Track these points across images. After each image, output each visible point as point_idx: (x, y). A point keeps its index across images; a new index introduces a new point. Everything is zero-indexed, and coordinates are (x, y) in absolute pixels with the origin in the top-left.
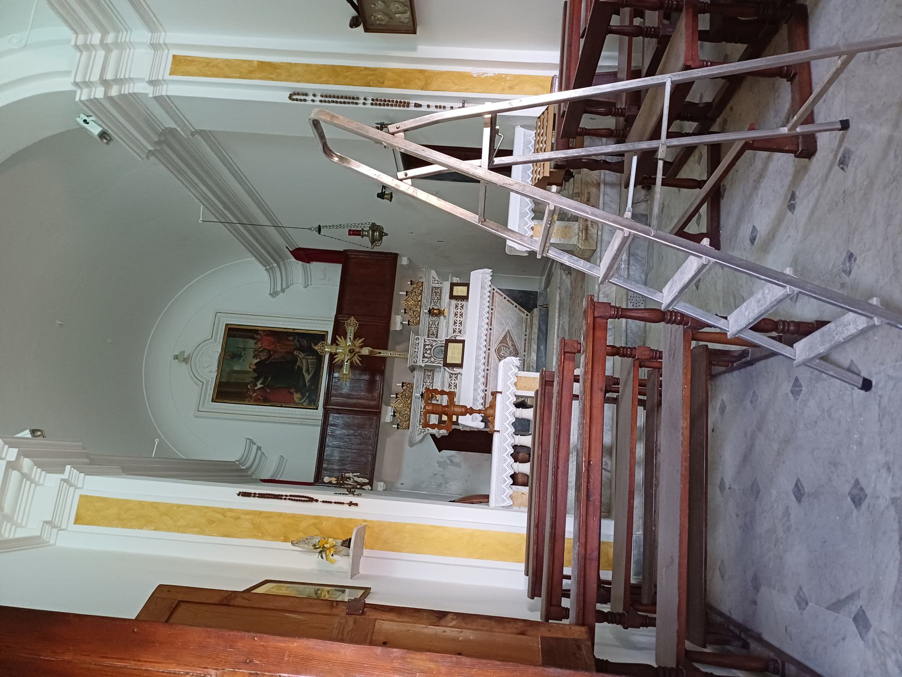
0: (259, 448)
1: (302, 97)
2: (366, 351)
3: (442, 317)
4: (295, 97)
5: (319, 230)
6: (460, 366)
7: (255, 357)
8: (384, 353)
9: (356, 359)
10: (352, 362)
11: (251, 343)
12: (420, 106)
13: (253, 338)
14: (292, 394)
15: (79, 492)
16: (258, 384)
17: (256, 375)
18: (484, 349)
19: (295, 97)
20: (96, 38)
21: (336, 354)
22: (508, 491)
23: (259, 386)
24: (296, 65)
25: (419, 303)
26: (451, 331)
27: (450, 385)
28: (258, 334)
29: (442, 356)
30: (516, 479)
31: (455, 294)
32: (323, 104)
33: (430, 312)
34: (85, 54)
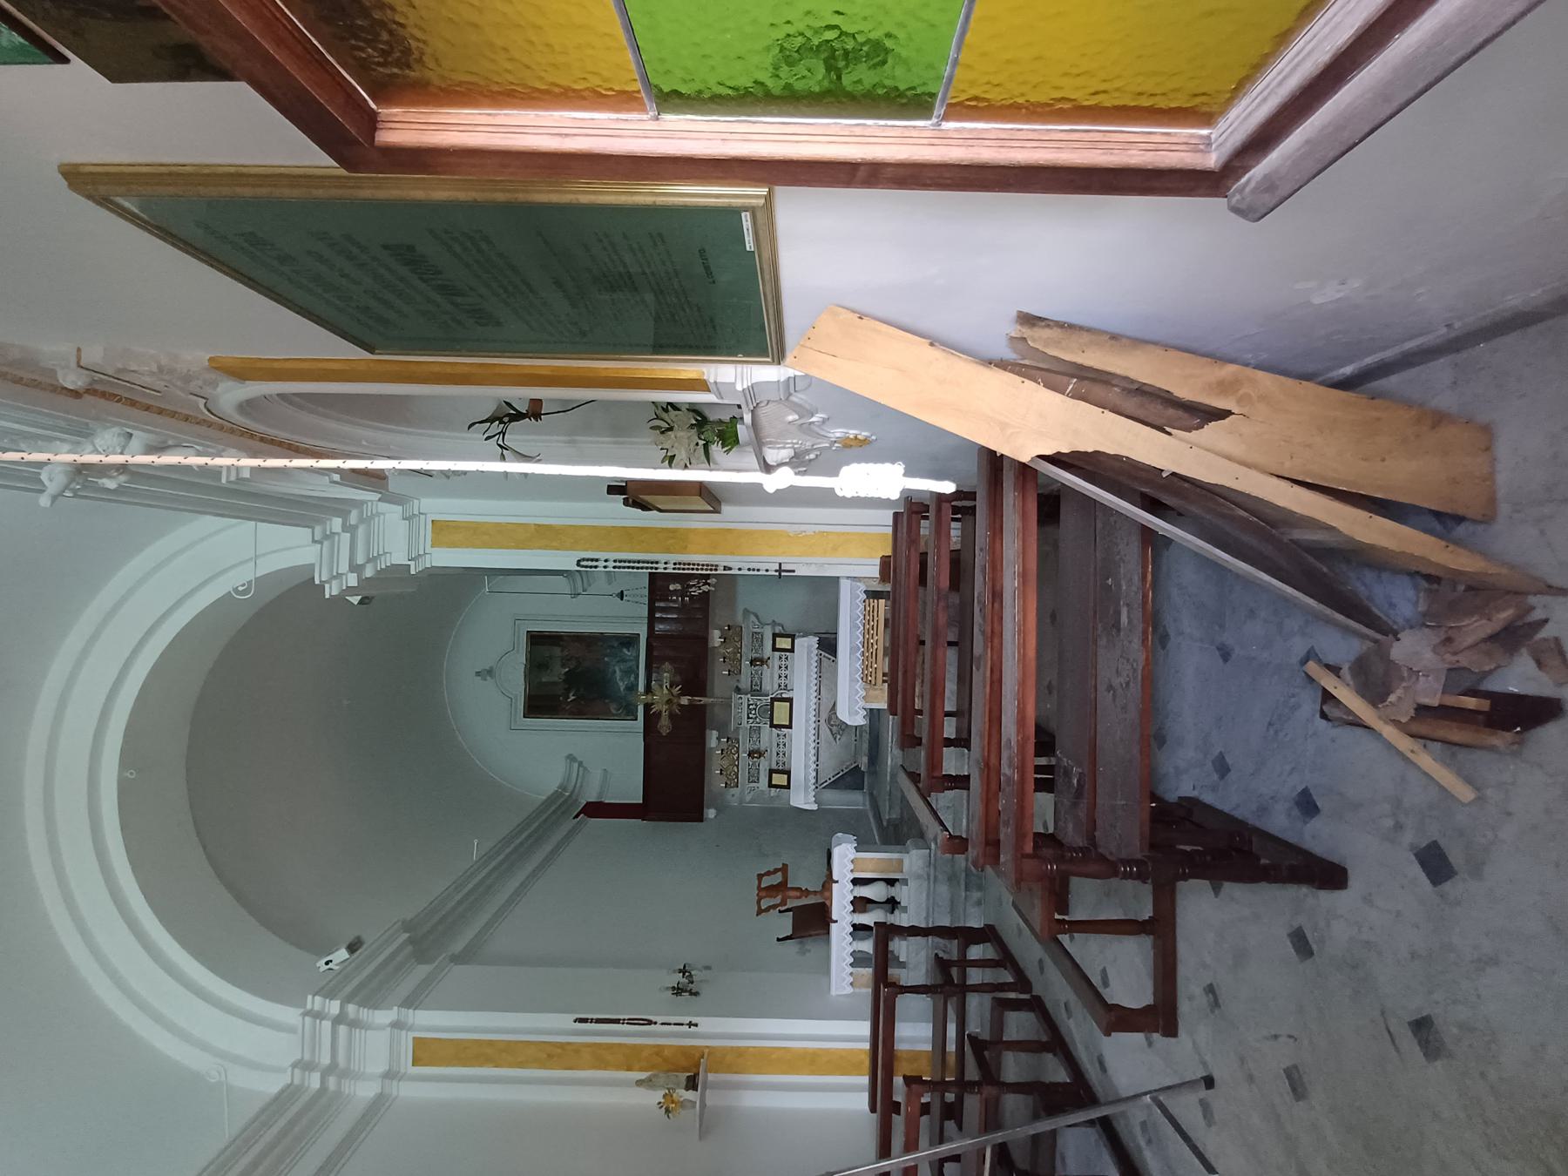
0: (580, 764)
2: (685, 701)
5: (621, 595)
6: (790, 727)
7: (563, 666)
8: (704, 700)
11: (557, 651)
15: (412, 1035)
20: (336, 524)
25: (738, 650)
30: (858, 929)
33: (752, 662)
34: (326, 543)
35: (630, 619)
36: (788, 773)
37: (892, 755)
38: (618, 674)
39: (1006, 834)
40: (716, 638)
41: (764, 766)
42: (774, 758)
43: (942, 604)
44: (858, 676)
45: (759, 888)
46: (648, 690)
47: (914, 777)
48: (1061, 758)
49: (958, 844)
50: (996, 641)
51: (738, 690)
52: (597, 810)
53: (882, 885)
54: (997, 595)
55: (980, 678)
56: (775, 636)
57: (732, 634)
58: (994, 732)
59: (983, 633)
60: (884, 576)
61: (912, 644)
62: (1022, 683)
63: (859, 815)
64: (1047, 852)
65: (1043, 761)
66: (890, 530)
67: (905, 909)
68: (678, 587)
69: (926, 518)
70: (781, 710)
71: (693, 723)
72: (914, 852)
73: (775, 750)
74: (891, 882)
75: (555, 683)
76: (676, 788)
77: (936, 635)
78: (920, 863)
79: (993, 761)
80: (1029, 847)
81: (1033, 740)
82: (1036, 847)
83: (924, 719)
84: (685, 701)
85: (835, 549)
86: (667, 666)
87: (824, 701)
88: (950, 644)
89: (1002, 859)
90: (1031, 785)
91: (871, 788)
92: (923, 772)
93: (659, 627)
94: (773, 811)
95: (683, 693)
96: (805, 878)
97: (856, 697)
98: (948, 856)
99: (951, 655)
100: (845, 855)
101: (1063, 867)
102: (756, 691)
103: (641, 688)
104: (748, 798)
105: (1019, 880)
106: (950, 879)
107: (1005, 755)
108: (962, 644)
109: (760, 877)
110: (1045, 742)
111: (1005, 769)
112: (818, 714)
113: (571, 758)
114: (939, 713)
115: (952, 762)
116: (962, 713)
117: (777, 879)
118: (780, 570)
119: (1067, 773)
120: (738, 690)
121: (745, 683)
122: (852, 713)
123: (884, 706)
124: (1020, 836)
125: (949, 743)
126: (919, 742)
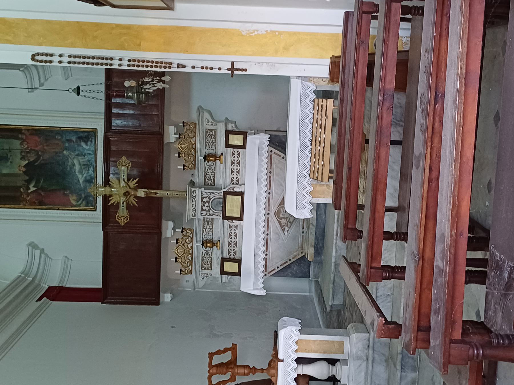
1: (49, 58)
2: (141, 193)
3: (215, 247)
4: (37, 58)
6: (241, 219)
7: (23, 158)
9: (133, 201)
11: (16, 144)
13: (17, 138)
14: (67, 195)
16: (31, 186)
17: (27, 178)
18: (265, 195)
21: (111, 196)
22: (308, 188)
23: (32, 189)
24: (34, 21)
26: (228, 181)
27: (229, 253)
29: (221, 209)
31: (231, 143)
32: (71, 65)
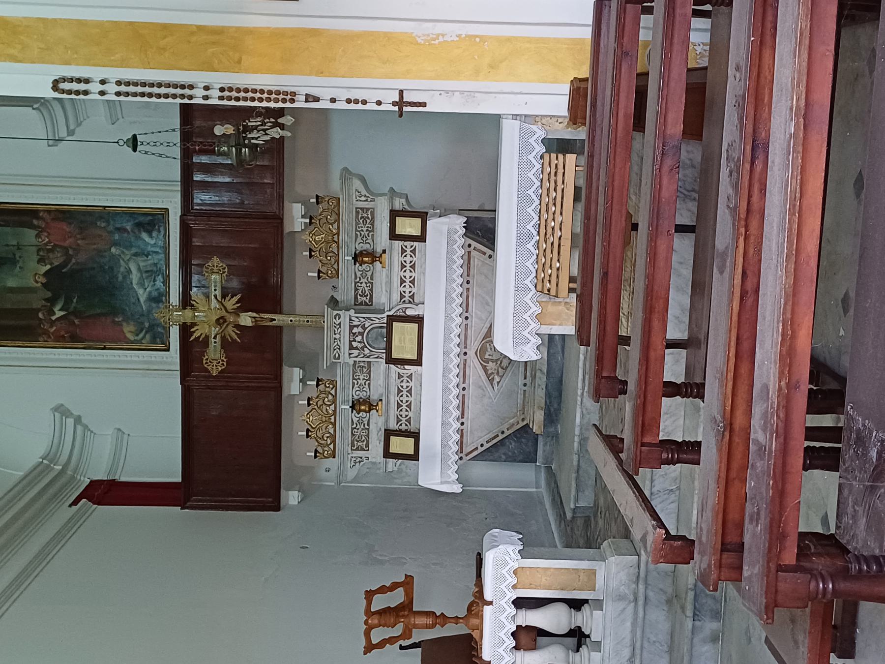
1: (82, 87)
2: (246, 319)
4: (62, 86)
6: (418, 362)
7: (41, 261)
8: (279, 319)
9: (232, 333)
10: (223, 339)
11: (29, 235)
12: (316, 99)
13: (32, 227)
14: (119, 324)
16: (56, 309)
19: (62, 86)
21: (194, 324)
23: (59, 314)
25: (333, 239)
27: (399, 420)
28: (38, 218)
29: (384, 345)
31: (399, 231)
35: (150, 181)
36: (416, 436)
37: (583, 409)
38: (135, 277)
39: (754, 535)
40: (296, 217)
41: (377, 422)
42: (393, 412)
43: (669, 162)
44: (529, 282)
45: (368, 613)
46: (186, 301)
47: (613, 444)
48: (855, 416)
49: (678, 549)
50: (754, 224)
51: (334, 303)
52: (107, 492)
53: (563, 608)
54: (758, 147)
55: (723, 288)
56: (394, 214)
57: (323, 210)
58: (744, 369)
59: (734, 211)
60: (576, 115)
61: (618, 225)
62: (793, 294)
63: (529, 501)
64: (820, 563)
65: (826, 420)
66: (587, 33)
67: (598, 646)
68: (229, 129)
69: (649, 11)
70: (404, 334)
71: (261, 357)
72: (613, 560)
73: (394, 399)
74: (576, 605)
75: (31, 290)
76: (233, 456)
77: (656, 214)
78: (623, 576)
79: (739, 420)
80: (790, 557)
81: (805, 386)
82: (802, 553)
83: (634, 350)
84: (246, 319)
85: (492, 66)
86: (216, 260)
87: (474, 321)
88: (681, 229)
89: (746, 573)
90: (797, 459)
91: (548, 461)
92: (627, 436)
93: (201, 198)
94: (392, 495)
95: (244, 306)
96: (439, 596)
97: (525, 315)
98: (670, 567)
99: (683, 246)
100: (505, 565)
101: (843, 586)
102: (364, 303)
103: (175, 298)
104: (351, 474)
105: (771, 607)
106: (669, 602)
107: (758, 410)
108: (698, 230)
109: (370, 595)
110: (827, 387)
111: (758, 434)
112: (464, 344)
113: (62, 411)
114: (657, 342)
115: (676, 420)
116: (692, 343)
117: (397, 598)
118: (401, 103)
119: (861, 441)
120: (334, 303)
121: (345, 292)
122: (518, 343)
123: (569, 329)
124: (777, 534)
125: (672, 390)
126: (621, 388)
